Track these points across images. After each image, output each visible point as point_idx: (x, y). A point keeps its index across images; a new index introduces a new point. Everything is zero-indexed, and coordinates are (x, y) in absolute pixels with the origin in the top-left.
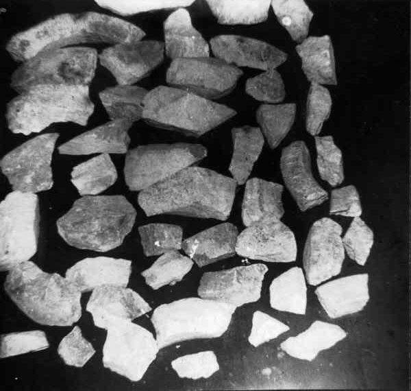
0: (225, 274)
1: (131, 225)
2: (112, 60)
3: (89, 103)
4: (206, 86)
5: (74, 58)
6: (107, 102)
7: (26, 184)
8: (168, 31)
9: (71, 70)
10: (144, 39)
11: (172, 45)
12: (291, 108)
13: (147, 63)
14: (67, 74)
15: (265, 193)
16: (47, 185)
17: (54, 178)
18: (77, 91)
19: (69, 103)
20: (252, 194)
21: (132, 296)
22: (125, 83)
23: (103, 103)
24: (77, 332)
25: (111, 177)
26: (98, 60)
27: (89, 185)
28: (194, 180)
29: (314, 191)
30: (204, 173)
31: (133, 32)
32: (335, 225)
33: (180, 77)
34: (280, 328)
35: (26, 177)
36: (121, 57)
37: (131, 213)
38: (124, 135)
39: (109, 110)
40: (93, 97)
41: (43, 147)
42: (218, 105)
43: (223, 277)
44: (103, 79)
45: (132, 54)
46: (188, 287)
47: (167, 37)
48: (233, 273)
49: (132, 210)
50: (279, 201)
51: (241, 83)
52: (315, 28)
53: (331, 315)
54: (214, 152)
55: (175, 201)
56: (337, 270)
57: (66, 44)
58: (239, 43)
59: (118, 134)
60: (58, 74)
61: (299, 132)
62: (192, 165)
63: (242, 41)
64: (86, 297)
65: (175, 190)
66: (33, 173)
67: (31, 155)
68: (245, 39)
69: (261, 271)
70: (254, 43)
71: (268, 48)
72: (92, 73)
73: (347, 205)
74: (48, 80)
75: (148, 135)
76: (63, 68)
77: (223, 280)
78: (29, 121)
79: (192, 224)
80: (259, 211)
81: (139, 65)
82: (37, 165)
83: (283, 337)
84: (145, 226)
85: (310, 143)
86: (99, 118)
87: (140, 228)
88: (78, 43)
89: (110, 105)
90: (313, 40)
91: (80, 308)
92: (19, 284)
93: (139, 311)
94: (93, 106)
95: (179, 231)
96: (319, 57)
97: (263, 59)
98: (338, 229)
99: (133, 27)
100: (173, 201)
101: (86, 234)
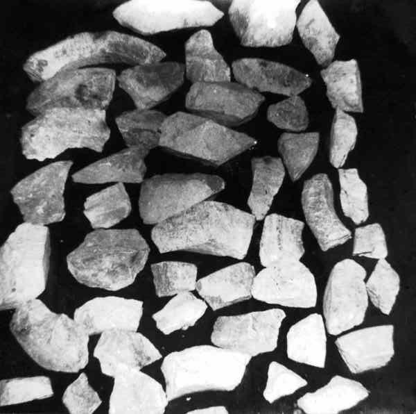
1: (144, 262)
2: (131, 83)
4: (226, 113)
6: (124, 128)
10: (164, 60)
11: (193, 68)
12: (314, 138)
13: (166, 85)
14: (83, 97)
15: (284, 230)
16: (59, 216)
17: (66, 209)
20: (270, 231)
21: (141, 341)
22: (143, 107)
23: (119, 129)
24: (83, 379)
26: (117, 83)
27: (101, 218)
28: (210, 216)
31: (153, 53)
34: (298, 382)
36: (139, 80)
38: (140, 163)
39: (125, 136)
40: (110, 123)
41: (57, 175)
42: (237, 134)
45: (152, 76)
46: (200, 334)
47: (188, 59)
51: (262, 110)
52: (342, 53)
53: (353, 370)
54: (233, 187)
55: (190, 237)
56: (360, 320)
58: (262, 67)
59: (134, 162)
60: (75, 97)
63: (265, 65)
64: (94, 340)
66: (45, 203)
67: (44, 183)
68: (267, 62)
70: (277, 67)
71: (291, 72)
72: (109, 96)
74: (65, 103)
76: (80, 90)
82: (50, 194)
83: (300, 393)
84: (158, 264)
85: (334, 176)
86: (115, 145)
90: (339, 65)
94: (109, 132)
95: (192, 270)
96: (346, 83)
97: (287, 84)
98: (362, 272)
99: (153, 47)
100: (187, 237)
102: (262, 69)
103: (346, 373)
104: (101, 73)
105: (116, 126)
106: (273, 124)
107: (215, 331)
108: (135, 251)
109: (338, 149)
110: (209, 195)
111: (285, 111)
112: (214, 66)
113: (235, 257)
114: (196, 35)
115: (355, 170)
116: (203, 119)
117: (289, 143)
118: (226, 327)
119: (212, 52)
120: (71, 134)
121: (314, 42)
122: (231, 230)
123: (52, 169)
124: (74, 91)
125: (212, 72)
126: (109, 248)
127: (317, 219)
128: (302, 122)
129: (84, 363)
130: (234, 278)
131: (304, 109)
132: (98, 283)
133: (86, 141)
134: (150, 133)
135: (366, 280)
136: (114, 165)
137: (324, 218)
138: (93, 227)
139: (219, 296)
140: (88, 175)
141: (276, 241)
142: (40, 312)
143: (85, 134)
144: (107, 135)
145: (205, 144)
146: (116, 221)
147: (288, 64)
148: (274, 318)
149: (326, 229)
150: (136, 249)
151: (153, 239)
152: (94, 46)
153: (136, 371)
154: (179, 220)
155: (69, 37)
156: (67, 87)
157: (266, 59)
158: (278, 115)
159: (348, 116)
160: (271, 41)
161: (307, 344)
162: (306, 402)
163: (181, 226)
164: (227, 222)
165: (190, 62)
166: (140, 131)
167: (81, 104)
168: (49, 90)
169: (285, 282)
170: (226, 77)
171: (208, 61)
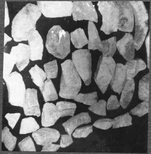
0: (36, 100)
1: (57, 57)
2: (127, 39)
3: (110, 32)
4: (115, 81)
5: (129, 24)
6: (110, 40)
7: (76, 8)
8: (138, 61)
9: (124, 22)
10: (135, 50)
11: (132, 63)
12: (104, 114)
13: (126, 54)
14: (123, 20)
15: (70, 110)
17: (78, 21)
18: (116, 27)
19: (110, 24)
20: (70, 106)
21: (26, 63)
22: (117, 45)
23: (110, 39)
25: (78, 46)
26: (128, 32)
27: (75, 37)
29: (70, 130)
30: (79, 88)
31: (138, 46)
32: (57, 116)
33: (119, 70)
35: (79, 8)
36: (128, 43)
37: (62, 57)
38: (96, 48)
39: (107, 41)
40: (112, 34)
42: (107, 87)
43: (35, 99)
44: (119, 35)
45: (129, 47)
46: (29, 83)
47: (136, 61)
48: (36, 104)
49: (64, 57)
50: (117, 72)
51: (116, 94)
52: (135, 118)
53: (19, 144)
54: (86, 88)
56: (38, 143)
57: (136, 17)
58: (131, 91)
59: (96, 46)
60: (123, 17)
61: (95, 118)
62: (82, 80)
63: (132, 92)
64: (26, 43)
65: (72, 76)
66: (80, 12)
68: (133, 93)
69: (38, 114)
70: (131, 96)
72: (122, 30)
73: (65, 143)
74: (121, 13)
75: (95, 57)
76: (125, 19)
77: (33, 100)
78: (103, 6)
79: (57, 82)
80: (63, 109)
81: (125, 51)
82: (84, 14)
83: (9, 127)
85: (90, 124)
86: (103, 36)
87: (56, 61)
88: (135, 22)
89: (109, 42)
90: (130, 118)
91: (20, 41)
92: (31, 11)
93: (19, 67)
95: (55, 76)
96: (124, 121)
98: (56, 140)
99: (141, 46)
101: (53, 39)
102: (130, 91)
103: (18, 141)
104: (132, 26)
105: (111, 37)
106: (109, 97)
107: (31, 90)
108: (62, 54)
109: (100, 125)
110: (84, 80)
111: (114, 102)
112: (132, 73)
113: (42, 50)
114: (145, 64)
115: (92, 131)
116: (113, 75)
117: (103, 104)
118: (33, 94)
119: (138, 71)
120: (108, 18)
121: (139, 108)
122: (71, 91)
123: (94, 13)
124: (126, 17)
125: (130, 72)
126: (63, 44)
127: (74, 121)
128: (110, 108)
129: (16, 40)
130: (52, 96)
131: (115, 108)
132: (49, 40)
133: (105, 24)
134: (108, 50)
135: (53, 143)
136: (96, 40)
137: (75, 124)
138: (71, 34)
139: (45, 90)
140: (92, 29)
141: (65, 108)
142: (36, 17)
143: (108, 24)
144: (107, 33)
145: (103, 75)
146: (73, 43)
147: (132, 100)
148: (37, 113)
149: (71, 126)
150: (62, 55)
151: (67, 60)
152: (143, 22)
153: (15, 63)
154: (74, 71)
155: (147, 11)
156: (127, 14)
157: (134, 92)
158: (113, 99)
159: (111, 125)
160: (141, 92)
161: (28, 126)
162: (7, 130)
163: (71, 72)
164: (73, 90)
165: (134, 62)
166: (109, 47)
167: (120, 19)
168: (126, 5)
169: (51, 115)
170: (128, 78)
171: (134, 70)
